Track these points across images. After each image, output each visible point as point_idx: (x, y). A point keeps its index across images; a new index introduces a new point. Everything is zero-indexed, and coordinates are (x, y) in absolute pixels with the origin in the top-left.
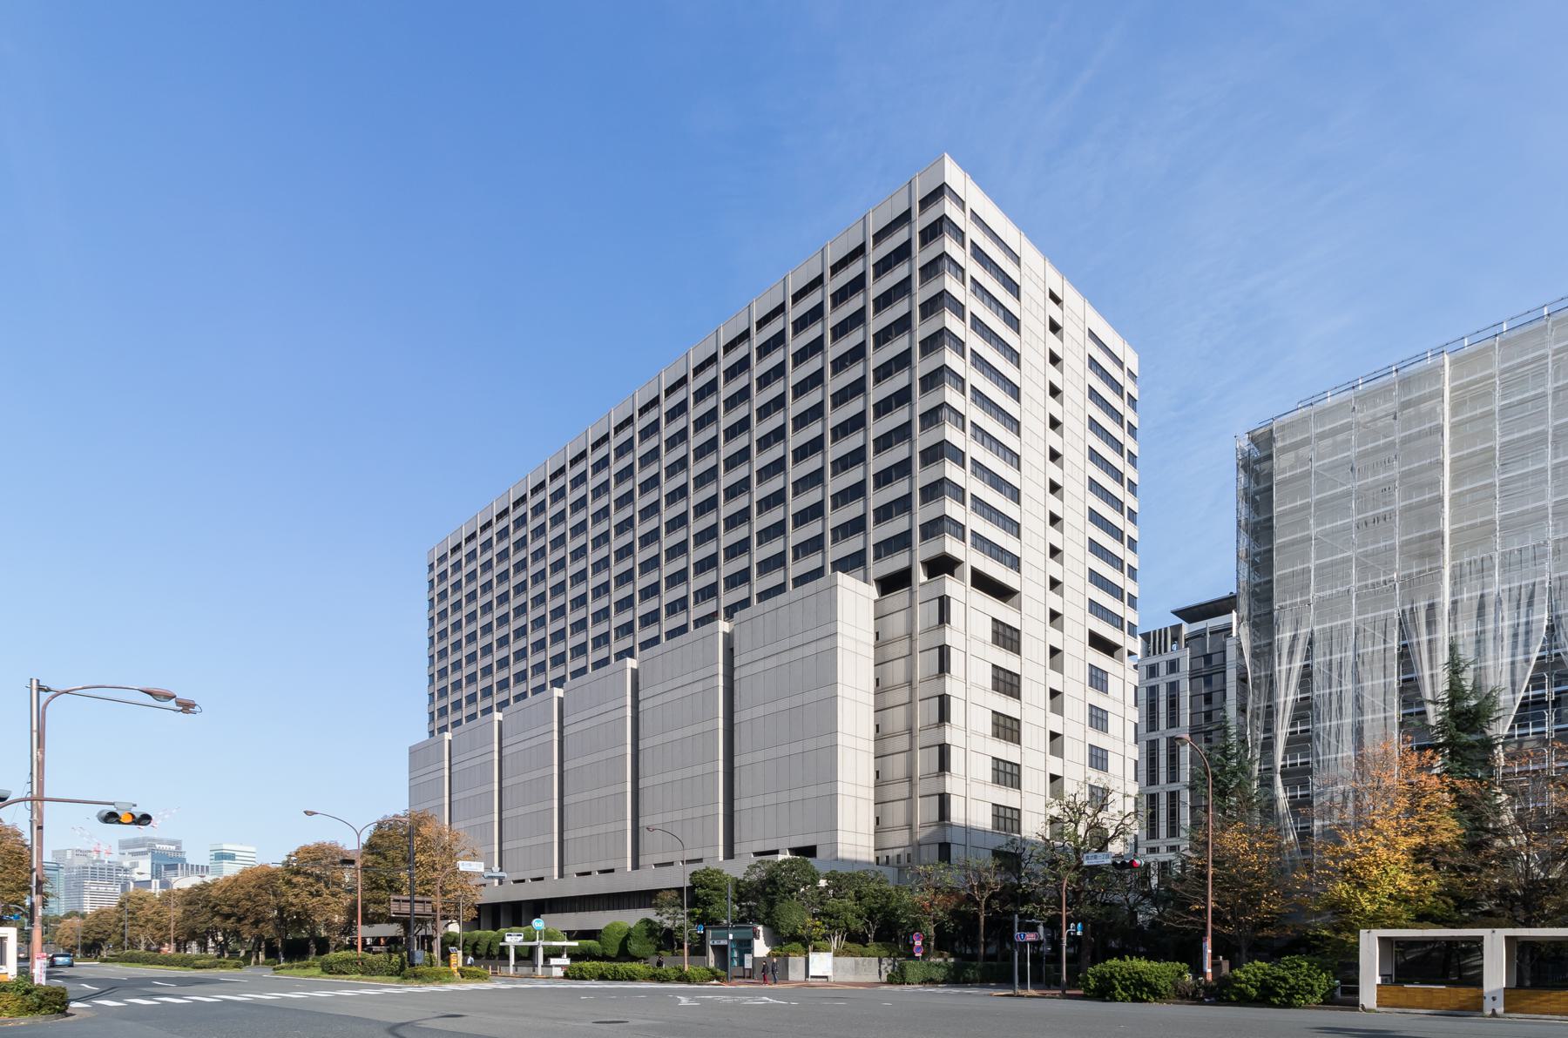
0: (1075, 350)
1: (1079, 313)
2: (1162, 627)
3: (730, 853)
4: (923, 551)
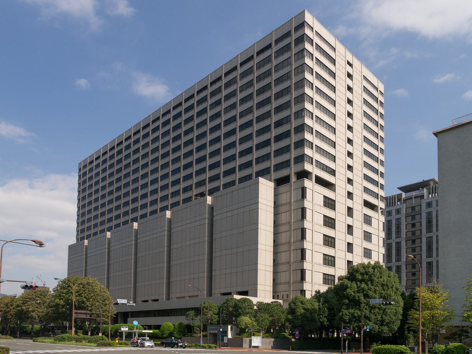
0: (357, 84)
1: (359, 69)
2: (393, 194)
3: (210, 294)
4: (294, 169)
